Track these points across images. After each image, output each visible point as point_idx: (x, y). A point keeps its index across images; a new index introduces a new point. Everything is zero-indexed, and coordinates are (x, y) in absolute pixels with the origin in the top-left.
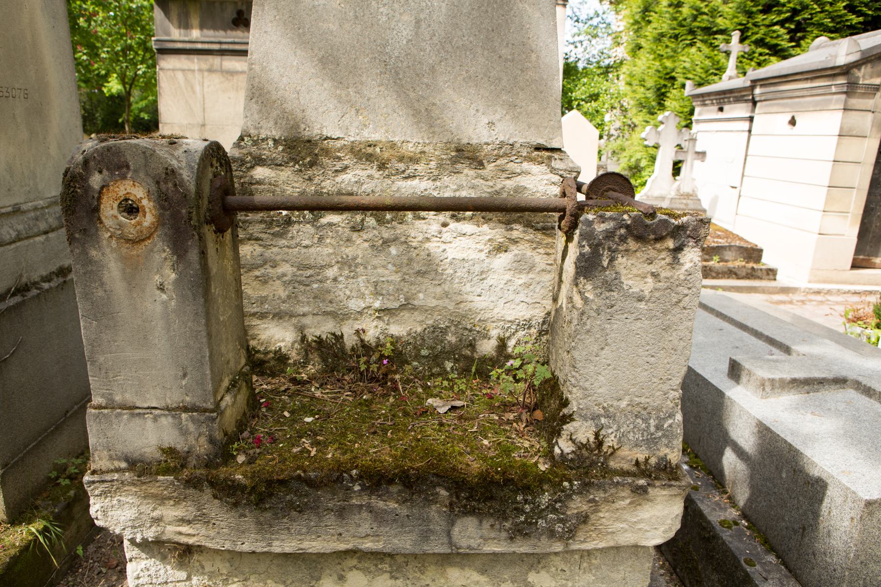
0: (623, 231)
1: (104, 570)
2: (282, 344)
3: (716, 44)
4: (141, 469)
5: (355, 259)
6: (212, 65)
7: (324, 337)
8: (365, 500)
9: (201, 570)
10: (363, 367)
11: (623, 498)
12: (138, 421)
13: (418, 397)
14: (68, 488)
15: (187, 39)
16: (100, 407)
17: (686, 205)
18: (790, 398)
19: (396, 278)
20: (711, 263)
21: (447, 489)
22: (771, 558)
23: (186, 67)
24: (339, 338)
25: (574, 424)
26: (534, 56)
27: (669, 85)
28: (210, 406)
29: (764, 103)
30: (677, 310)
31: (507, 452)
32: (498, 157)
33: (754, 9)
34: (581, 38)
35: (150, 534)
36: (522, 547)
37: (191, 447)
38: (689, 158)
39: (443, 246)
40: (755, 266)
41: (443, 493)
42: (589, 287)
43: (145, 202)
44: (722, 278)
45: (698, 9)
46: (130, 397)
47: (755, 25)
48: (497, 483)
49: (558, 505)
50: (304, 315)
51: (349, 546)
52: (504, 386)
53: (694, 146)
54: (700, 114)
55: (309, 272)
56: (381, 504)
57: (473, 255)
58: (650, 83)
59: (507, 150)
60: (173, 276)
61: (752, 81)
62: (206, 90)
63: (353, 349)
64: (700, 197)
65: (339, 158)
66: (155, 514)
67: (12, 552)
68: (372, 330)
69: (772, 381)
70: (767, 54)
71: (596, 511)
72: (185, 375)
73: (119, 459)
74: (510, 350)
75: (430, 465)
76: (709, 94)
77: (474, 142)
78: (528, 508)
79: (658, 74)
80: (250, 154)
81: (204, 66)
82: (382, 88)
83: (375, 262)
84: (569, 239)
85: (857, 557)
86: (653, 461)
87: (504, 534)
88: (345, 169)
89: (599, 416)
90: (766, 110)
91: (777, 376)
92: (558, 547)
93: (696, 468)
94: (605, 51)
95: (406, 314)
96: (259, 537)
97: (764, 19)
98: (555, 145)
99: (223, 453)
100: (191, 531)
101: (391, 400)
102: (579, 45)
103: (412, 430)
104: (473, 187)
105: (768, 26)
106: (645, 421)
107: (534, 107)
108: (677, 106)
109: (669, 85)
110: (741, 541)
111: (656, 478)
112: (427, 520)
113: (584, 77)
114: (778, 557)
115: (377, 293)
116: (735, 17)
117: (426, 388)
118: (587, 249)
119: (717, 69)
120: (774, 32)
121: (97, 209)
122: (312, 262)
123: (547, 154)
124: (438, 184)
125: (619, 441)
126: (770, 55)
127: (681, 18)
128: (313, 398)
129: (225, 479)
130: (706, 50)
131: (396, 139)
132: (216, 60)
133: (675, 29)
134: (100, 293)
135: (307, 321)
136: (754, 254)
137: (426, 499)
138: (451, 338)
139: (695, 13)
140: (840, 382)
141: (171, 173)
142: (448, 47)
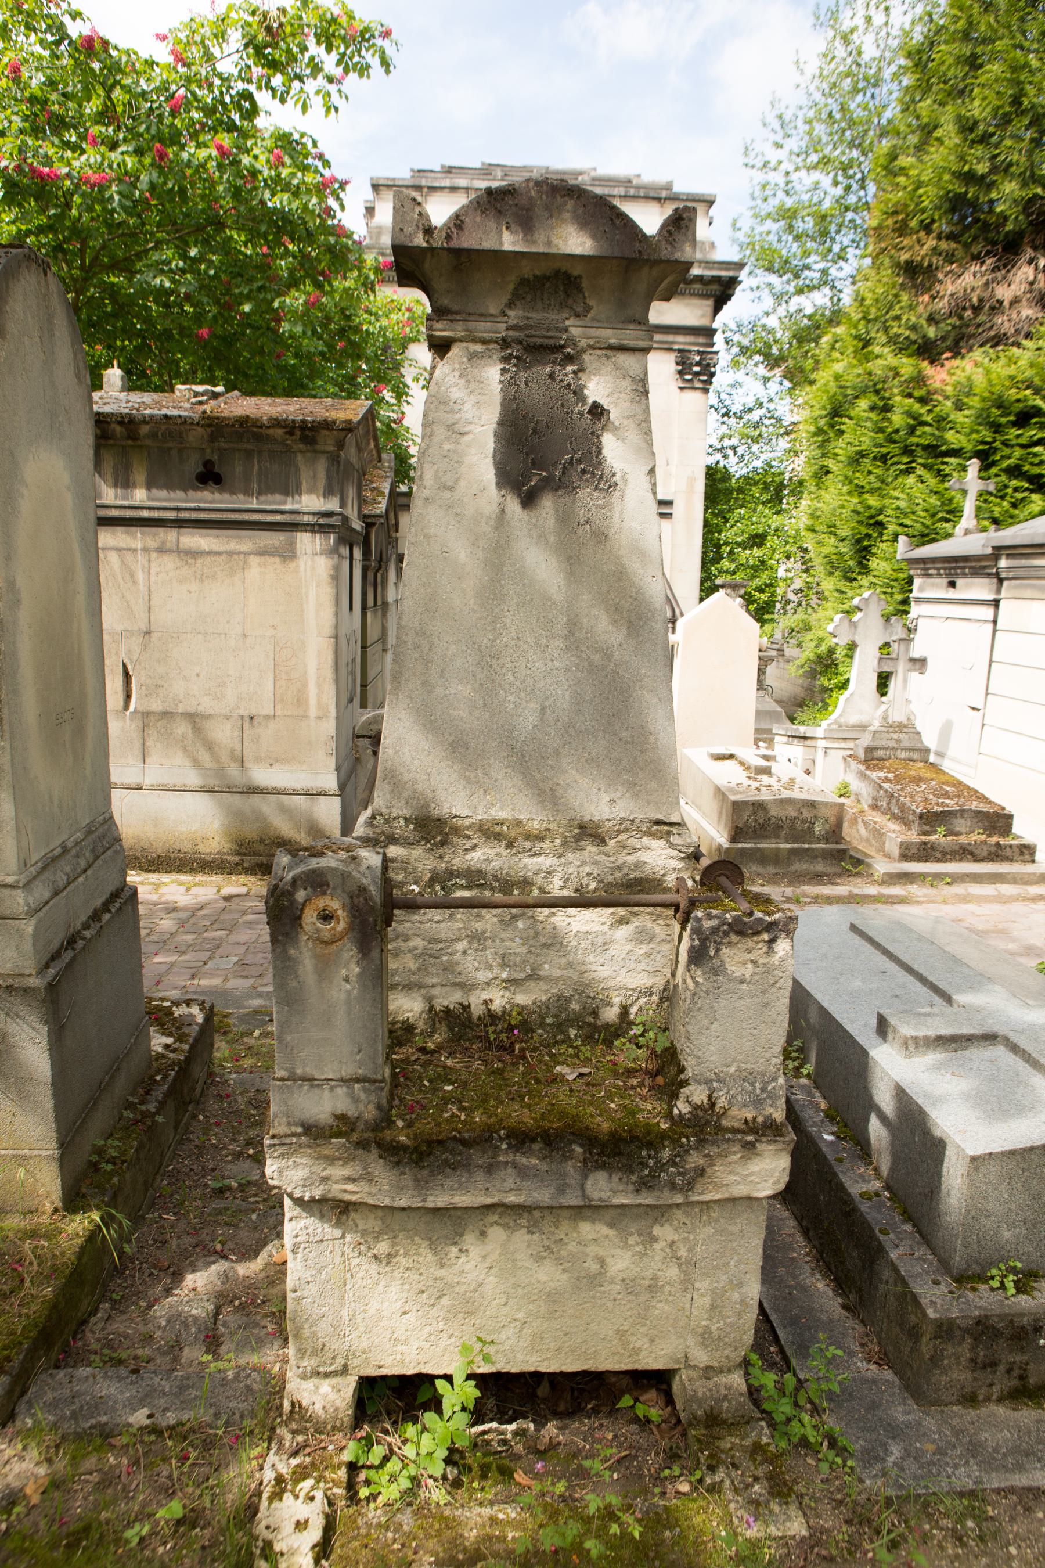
0: (726, 927)
1: (155, 1272)
2: (410, 1015)
3: (947, 471)
4: (314, 1133)
5: (484, 932)
6: (164, 542)
7: (452, 1007)
8: (510, 1157)
9: (355, 1228)
10: (492, 1037)
11: (735, 1153)
12: (316, 1091)
13: (546, 1064)
14: (111, 1174)
15: (126, 503)
16: (282, 1079)
17: (899, 741)
18: (933, 1057)
19: (523, 950)
20: (933, 838)
21: (582, 1146)
22: (908, 1227)
23: (123, 545)
24: (466, 1008)
25: (690, 1088)
26: (652, 738)
27: (875, 535)
28: (379, 1077)
29: (1014, 582)
30: (773, 990)
31: (633, 1113)
32: (619, 832)
33: (1003, 420)
34: (734, 441)
35: (317, 1193)
36: (647, 1199)
37: (361, 1113)
38: (901, 667)
39: (568, 920)
40: (1002, 841)
41: (578, 1149)
42: (699, 973)
43: (340, 912)
44: (951, 861)
45: (915, 417)
46: (310, 1070)
47: (1005, 444)
48: (625, 1140)
49: (678, 1159)
50: (433, 986)
51: (495, 1200)
52: (627, 1054)
53: (907, 650)
54: (921, 589)
55: (440, 946)
56: (524, 1161)
57: (597, 928)
58: (844, 532)
59: (628, 826)
60: (357, 970)
61: (994, 548)
62: (152, 579)
63: (479, 1018)
64: (919, 729)
65: (469, 837)
66: (324, 1174)
67: (80, 1241)
68: (499, 1000)
69: (915, 1039)
70: (1027, 489)
71: (712, 1165)
72: (359, 1051)
73: (296, 1125)
74: (632, 1017)
75: (567, 1126)
76: (934, 560)
77: (596, 818)
78: (651, 1162)
79: (856, 518)
80: (383, 833)
81: (152, 544)
82: (509, 770)
83: (503, 935)
84: (683, 928)
85: (968, 1212)
86: (760, 1119)
87: (631, 1187)
88: (474, 847)
89: (711, 1081)
90: (1017, 594)
91: (921, 1033)
92: (679, 1199)
93: (844, 1139)
94: (773, 463)
95: (531, 984)
96: (415, 1193)
97: (1018, 436)
98: (674, 819)
99: (385, 1120)
100: (355, 1189)
101: (521, 1068)
102: (730, 453)
103: (546, 1095)
104: (596, 863)
105: (1023, 446)
106: (752, 1084)
107: (653, 785)
108: (888, 568)
109: (875, 535)
110: (879, 1211)
111: (763, 1135)
112: (563, 1175)
113: (741, 507)
114: (914, 1226)
115: (504, 965)
116: (973, 431)
117: (552, 1056)
118: (697, 942)
119: (949, 512)
120: (1035, 455)
121: (300, 918)
122: (443, 936)
123: (666, 828)
124: (563, 860)
125: (730, 1102)
126: (1032, 491)
127: (890, 430)
128: (445, 1067)
129: (392, 1141)
130: (932, 481)
131: (522, 817)
132: (170, 536)
133: (881, 446)
134: (294, 984)
135: (435, 992)
136: (999, 821)
137: (563, 1155)
138: (575, 1006)
139: (912, 422)
140: (990, 1038)
141: (363, 890)
142: (572, 731)
